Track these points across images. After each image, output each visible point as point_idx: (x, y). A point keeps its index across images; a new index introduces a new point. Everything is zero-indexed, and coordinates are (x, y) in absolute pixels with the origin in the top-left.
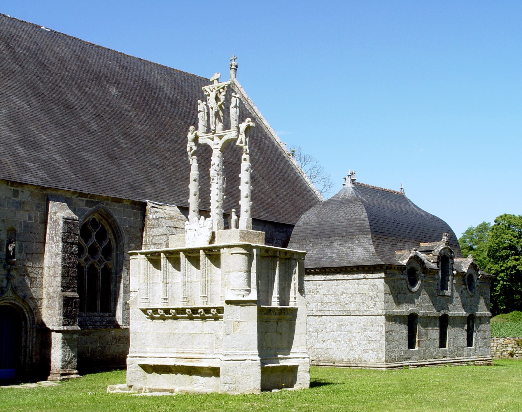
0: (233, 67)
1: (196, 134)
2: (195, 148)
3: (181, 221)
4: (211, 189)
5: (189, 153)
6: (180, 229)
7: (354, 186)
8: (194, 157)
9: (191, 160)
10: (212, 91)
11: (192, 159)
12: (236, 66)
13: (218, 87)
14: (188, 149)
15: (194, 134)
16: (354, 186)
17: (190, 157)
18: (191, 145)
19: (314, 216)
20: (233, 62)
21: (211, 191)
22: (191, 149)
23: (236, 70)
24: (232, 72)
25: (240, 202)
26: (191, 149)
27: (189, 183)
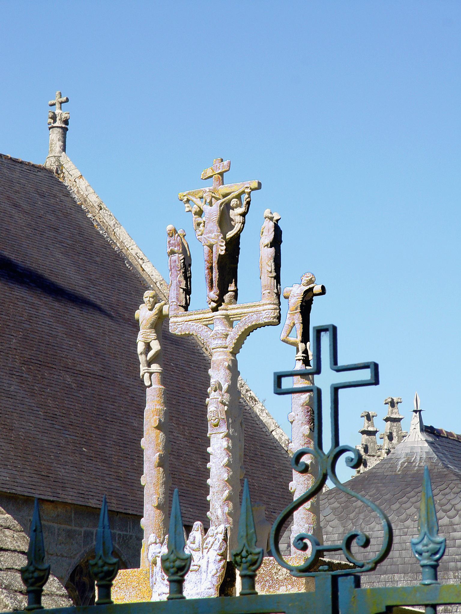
0: (58, 123)
1: (161, 310)
2: (156, 346)
3: (7, 532)
4: (209, 450)
5: (142, 359)
6: (9, 554)
7: (430, 439)
8: (155, 367)
9: (147, 376)
10: (211, 204)
11: (151, 374)
12: (66, 122)
13: (224, 196)
14: (141, 347)
15: (155, 311)
16: (430, 439)
17: (143, 368)
18: (146, 340)
19: (332, 517)
20: (58, 111)
21: (209, 455)
22: (148, 347)
23: (65, 130)
24: (55, 136)
25: (291, 484)
26: (148, 347)
27: (142, 436)
